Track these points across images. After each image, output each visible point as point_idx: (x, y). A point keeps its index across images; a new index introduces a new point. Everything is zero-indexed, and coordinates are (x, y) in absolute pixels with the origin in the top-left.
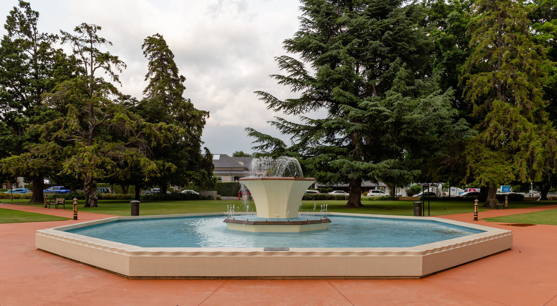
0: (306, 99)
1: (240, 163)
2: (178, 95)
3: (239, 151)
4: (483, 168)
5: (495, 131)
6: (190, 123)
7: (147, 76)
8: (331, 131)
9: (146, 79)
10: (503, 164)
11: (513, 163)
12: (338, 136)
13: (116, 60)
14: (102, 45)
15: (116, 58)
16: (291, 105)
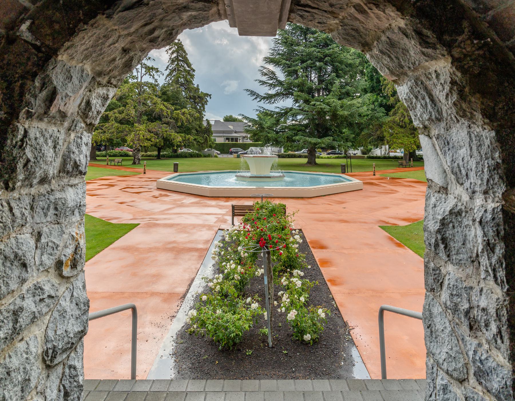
0: (277, 95)
1: (230, 126)
2: (189, 82)
3: (229, 115)
4: (395, 140)
5: (402, 116)
6: (196, 101)
7: (167, 68)
8: (294, 115)
9: (166, 70)
10: (408, 137)
11: (414, 137)
12: (299, 117)
13: (157, 71)
14: (149, 61)
15: (157, 69)
16: (269, 97)
